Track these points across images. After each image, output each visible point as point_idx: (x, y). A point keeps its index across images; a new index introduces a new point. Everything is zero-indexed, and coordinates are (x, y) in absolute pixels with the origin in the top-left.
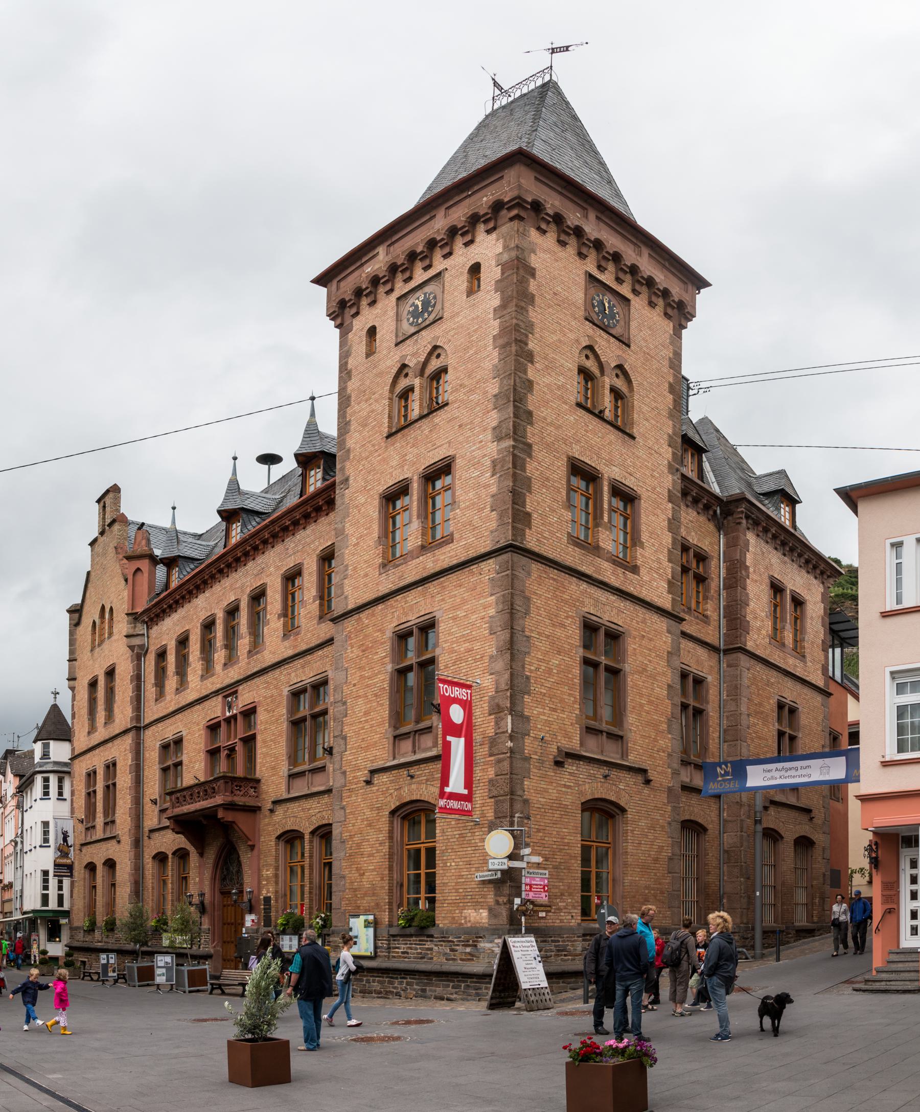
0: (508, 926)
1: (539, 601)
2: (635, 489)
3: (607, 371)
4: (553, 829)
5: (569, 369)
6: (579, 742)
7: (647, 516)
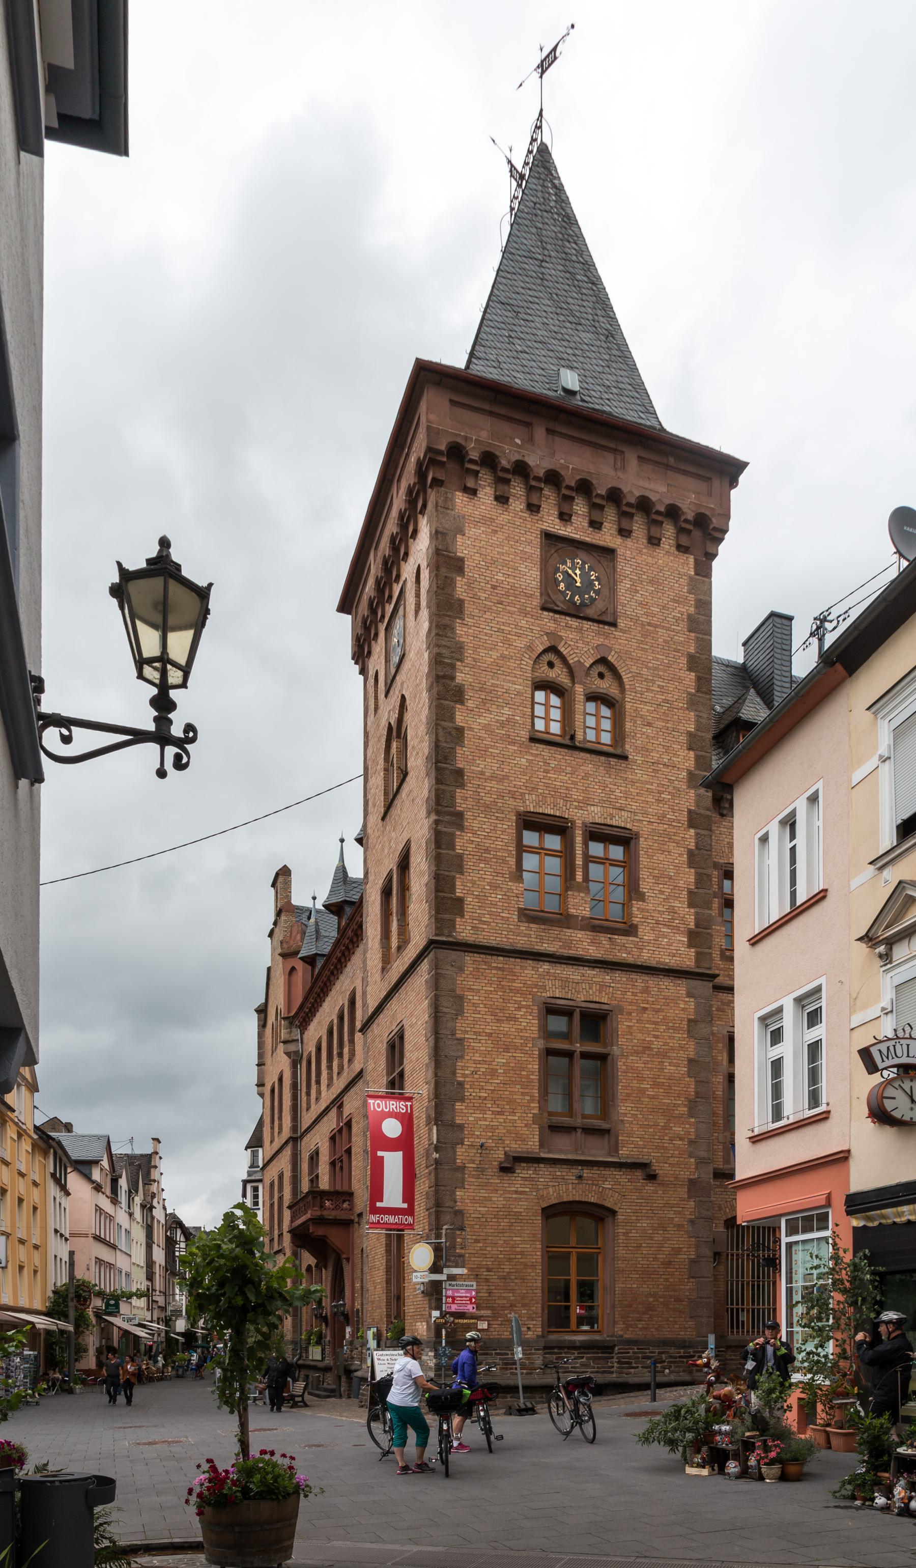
0: (434, 1339)
1: (475, 998)
2: (628, 826)
3: (579, 674)
4: (498, 1238)
5: (519, 693)
6: (538, 1144)
7: (650, 857)
